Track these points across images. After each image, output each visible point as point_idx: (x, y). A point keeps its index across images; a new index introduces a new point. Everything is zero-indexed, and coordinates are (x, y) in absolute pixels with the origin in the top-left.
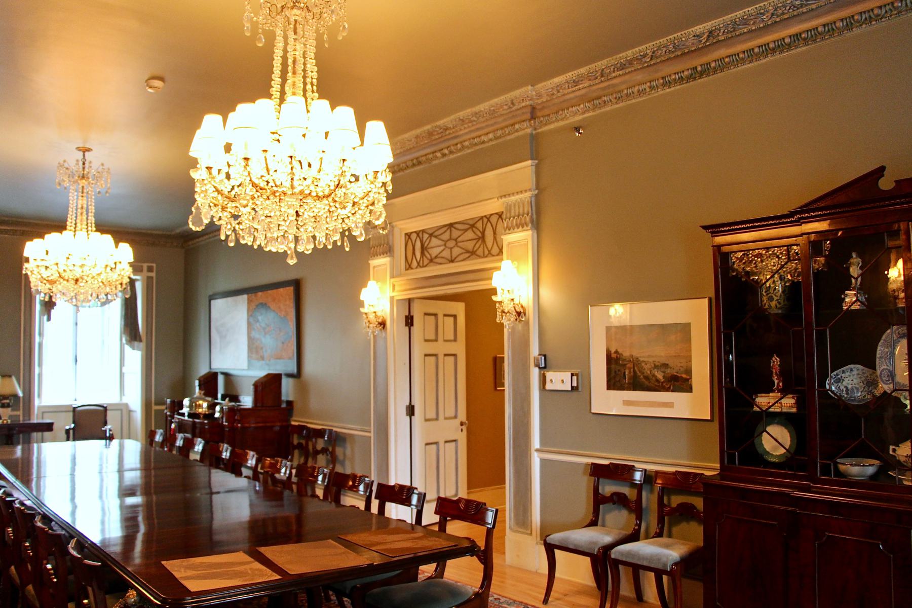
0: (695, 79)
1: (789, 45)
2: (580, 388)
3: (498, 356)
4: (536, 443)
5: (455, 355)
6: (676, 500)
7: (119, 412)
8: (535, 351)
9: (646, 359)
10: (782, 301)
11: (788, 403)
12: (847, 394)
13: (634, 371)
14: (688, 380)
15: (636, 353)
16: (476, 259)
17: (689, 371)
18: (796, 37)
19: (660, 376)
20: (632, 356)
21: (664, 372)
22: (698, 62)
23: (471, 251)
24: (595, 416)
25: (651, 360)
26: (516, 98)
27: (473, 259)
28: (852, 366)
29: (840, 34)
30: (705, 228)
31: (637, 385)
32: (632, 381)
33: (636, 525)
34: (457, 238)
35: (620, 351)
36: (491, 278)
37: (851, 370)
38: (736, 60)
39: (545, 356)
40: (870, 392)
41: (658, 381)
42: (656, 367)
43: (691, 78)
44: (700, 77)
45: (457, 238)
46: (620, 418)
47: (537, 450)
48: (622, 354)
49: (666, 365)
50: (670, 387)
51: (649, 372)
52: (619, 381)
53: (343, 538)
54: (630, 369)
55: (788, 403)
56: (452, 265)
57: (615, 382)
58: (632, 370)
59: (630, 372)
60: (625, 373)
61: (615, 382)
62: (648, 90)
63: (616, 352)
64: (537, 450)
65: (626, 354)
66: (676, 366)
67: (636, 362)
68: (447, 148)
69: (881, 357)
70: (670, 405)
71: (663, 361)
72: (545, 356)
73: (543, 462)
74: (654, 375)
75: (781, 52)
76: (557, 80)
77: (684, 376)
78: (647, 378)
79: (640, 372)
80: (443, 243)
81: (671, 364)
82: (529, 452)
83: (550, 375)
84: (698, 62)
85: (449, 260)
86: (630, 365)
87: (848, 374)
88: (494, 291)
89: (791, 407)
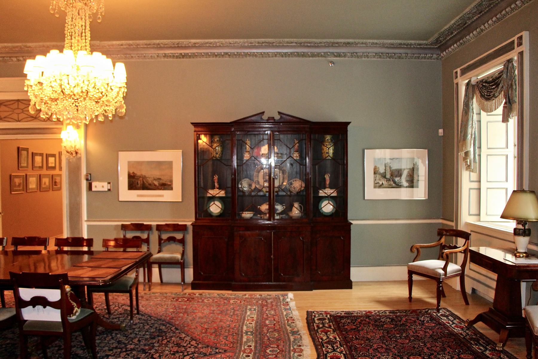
0: (180, 58)
1: (223, 56)
2: (113, 191)
3: (13, 174)
4: (85, 216)
5: (487, 182)
6: (165, 236)
7: (471, 190)
8: (84, 172)
9: (149, 176)
10: (220, 155)
11: (222, 194)
12: (294, 189)
13: (143, 182)
14: (170, 185)
15: (144, 173)
16: (38, 121)
17: (171, 181)
18: (227, 53)
19: (156, 183)
20: (142, 175)
21: (159, 182)
22: (183, 51)
23: (35, 117)
24: (120, 202)
25: (152, 177)
26: (142, 59)
27: (36, 122)
28: (245, 179)
29: (243, 57)
30: (192, 123)
31: (145, 187)
32: (142, 186)
33: (159, 248)
34: (23, 109)
35: (135, 172)
36: (60, 133)
37: (245, 180)
38: (201, 55)
39: (90, 174)
40: (250, 188)
41: (155, 185)
42: (155, 179)
43: (177, 57)
44: (183, 58)
45: (23, 109)
46: (125, 203)
47: (86, 221)
48: (136, 174)
49: (160, 179)
50: (162, 188)
51: (151, 182)
52: (135, 186)
53: (80, 265)
54: (140, 180)
55: (222, 194)
56: (18, 123)
57: (132, 186)
58: (142, 181)
59: (140, 182)
60: (138, 182)
61: (132, 186)
62: (156, 57)
63: (133, 173)
64: (86, 221)
65: (138, 173)
66: (165, 179)
67: (144, 177)
68: (23, 57)
69: (255, 176)
70: (139, 196)
71: (158, 177)
72: (90, 174)
73: (89, 226)
74: (153, 183)
75: (219, 57)
76: (114, 42)
77: (169, 183)
78: (150, 185)
79: (146, 182)
80: (24, 112)
81: (162, 178)
82: (81, 222)
83: (94, 184)
84: (183, 51)
85: (16, 120)
86: (141, 179)
87: (295, 182)
88: (61, 140)
89: (223, 194)
